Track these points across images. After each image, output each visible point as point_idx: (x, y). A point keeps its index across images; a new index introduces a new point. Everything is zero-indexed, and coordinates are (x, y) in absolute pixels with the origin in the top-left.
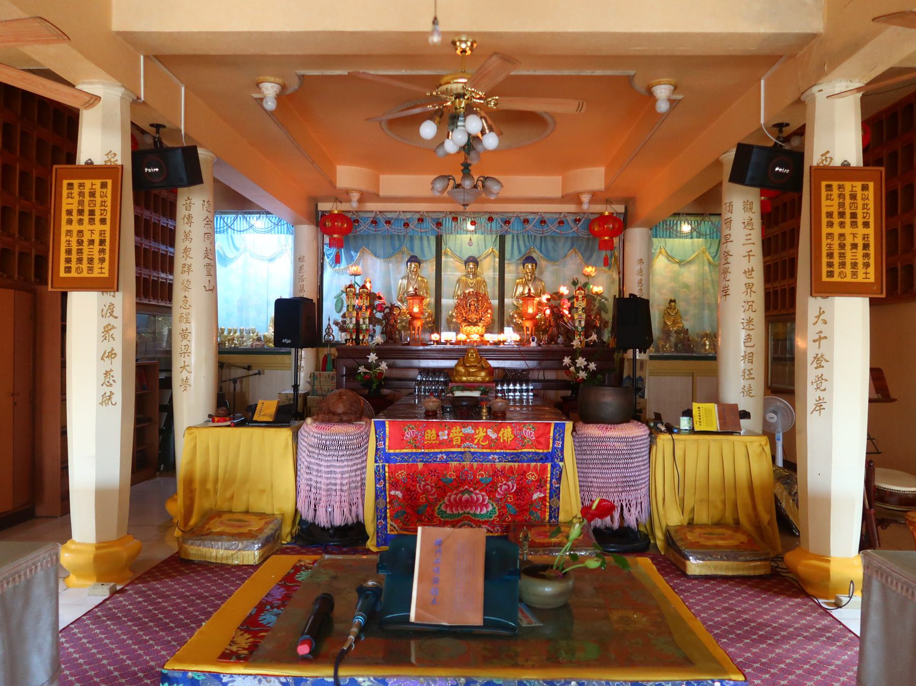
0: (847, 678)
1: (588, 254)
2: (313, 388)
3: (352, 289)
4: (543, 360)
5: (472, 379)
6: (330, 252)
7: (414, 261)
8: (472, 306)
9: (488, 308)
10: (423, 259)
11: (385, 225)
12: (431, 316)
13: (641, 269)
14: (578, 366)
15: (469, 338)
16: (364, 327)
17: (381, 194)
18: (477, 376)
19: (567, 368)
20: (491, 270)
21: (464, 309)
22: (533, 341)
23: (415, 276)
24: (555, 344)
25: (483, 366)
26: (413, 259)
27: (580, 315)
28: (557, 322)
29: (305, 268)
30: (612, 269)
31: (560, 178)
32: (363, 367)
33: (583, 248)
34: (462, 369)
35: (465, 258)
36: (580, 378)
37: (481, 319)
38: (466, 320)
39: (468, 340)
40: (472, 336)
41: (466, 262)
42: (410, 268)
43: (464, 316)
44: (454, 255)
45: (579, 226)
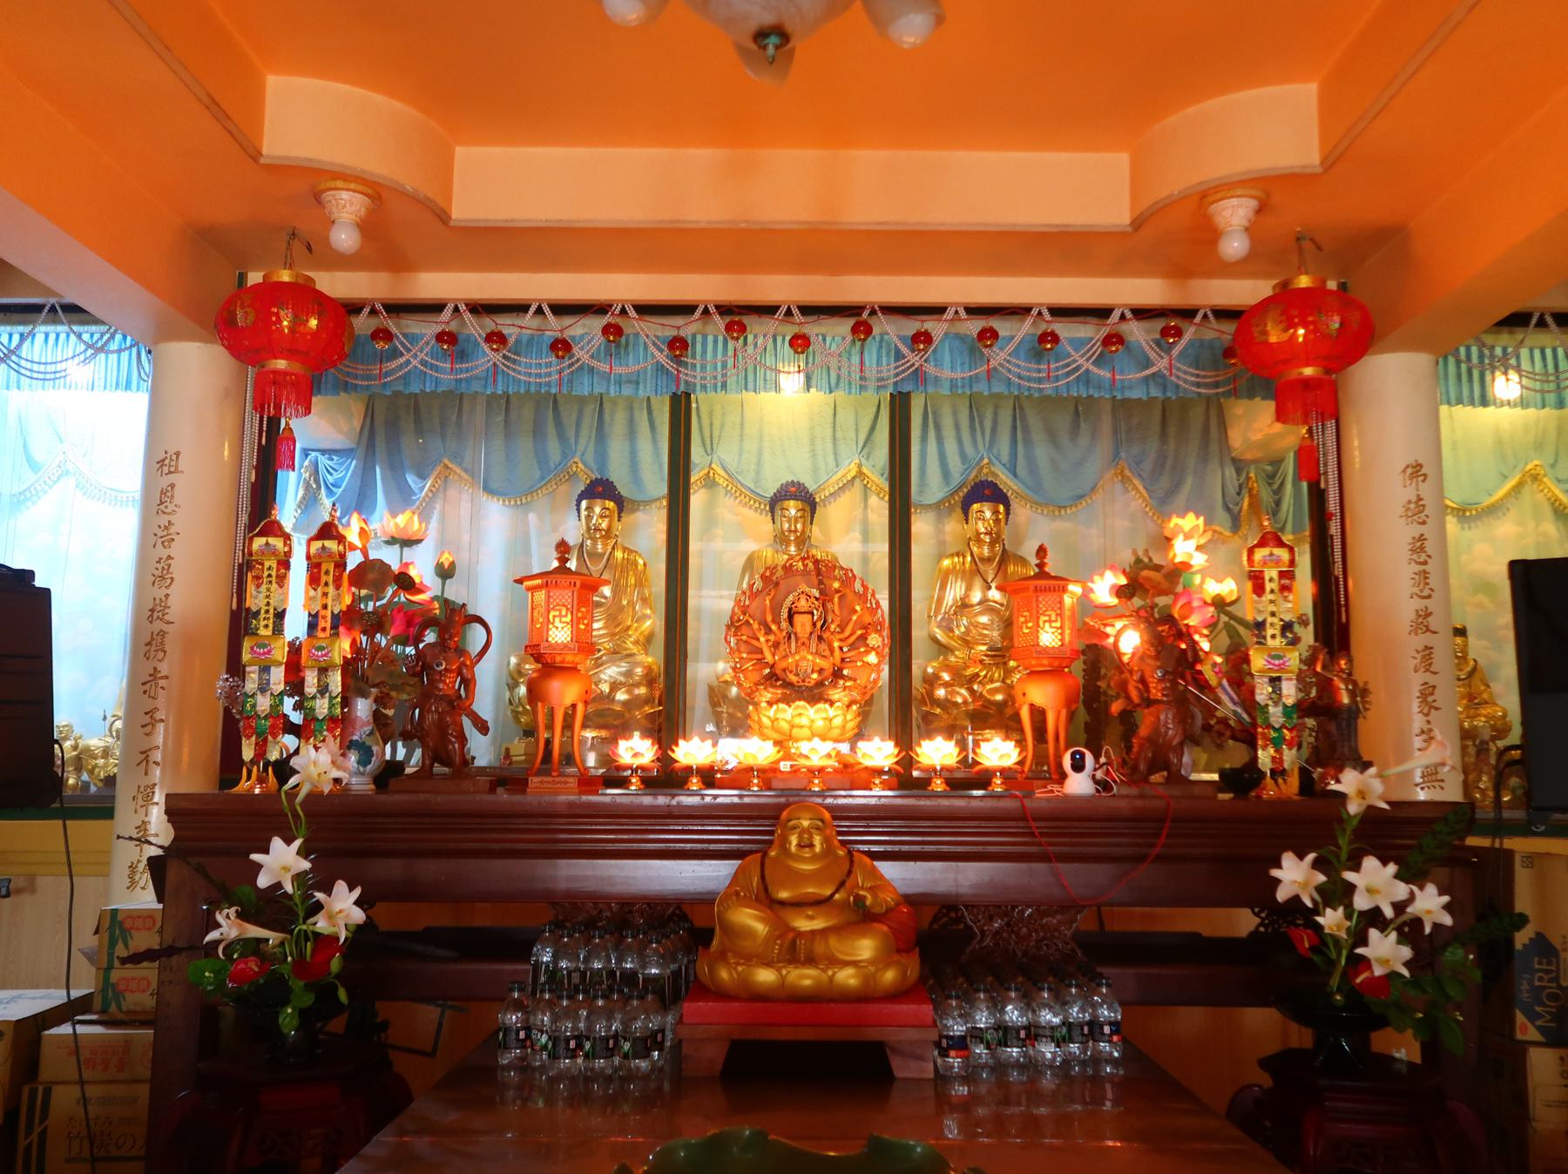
0: (886, 786)
1: (1164, 482)
2: (106, 979)
3: (272, 540)
4: (1141, 859)
5: (805, 978)
6: (337, 476)
8: (798, 619)
10: (639, 497)
11: (486, 347)
12: (650, 680)
13: (1420, 499)
14: (1361, 902)
15: (788, 756)
16: (263, 704)
17: (461, 211)
18: (835, 962)
20: (857, 535)
21: (769, 631)
22: (1078, 766)
23: (605, 545)
24: (1168, 780)
25: (860, 900)
26: (600, 489)
27: (1274, 655)
28: (1175, 684)
29: (180, 495)
30: (1244, 531)
31: (1122, 159)
32: (232, 911)
33: (1147, 465)
34: (750, 920)
35: (770, 490)
36: (1378, 971)
37: (837, 674)
38: (774, 678)
39: (785, 766)
40: (804, 747)
41: (775, 504)
42: (589, 518)
43: (769, 658)
44: (737, 488)
45: (1175, 352)
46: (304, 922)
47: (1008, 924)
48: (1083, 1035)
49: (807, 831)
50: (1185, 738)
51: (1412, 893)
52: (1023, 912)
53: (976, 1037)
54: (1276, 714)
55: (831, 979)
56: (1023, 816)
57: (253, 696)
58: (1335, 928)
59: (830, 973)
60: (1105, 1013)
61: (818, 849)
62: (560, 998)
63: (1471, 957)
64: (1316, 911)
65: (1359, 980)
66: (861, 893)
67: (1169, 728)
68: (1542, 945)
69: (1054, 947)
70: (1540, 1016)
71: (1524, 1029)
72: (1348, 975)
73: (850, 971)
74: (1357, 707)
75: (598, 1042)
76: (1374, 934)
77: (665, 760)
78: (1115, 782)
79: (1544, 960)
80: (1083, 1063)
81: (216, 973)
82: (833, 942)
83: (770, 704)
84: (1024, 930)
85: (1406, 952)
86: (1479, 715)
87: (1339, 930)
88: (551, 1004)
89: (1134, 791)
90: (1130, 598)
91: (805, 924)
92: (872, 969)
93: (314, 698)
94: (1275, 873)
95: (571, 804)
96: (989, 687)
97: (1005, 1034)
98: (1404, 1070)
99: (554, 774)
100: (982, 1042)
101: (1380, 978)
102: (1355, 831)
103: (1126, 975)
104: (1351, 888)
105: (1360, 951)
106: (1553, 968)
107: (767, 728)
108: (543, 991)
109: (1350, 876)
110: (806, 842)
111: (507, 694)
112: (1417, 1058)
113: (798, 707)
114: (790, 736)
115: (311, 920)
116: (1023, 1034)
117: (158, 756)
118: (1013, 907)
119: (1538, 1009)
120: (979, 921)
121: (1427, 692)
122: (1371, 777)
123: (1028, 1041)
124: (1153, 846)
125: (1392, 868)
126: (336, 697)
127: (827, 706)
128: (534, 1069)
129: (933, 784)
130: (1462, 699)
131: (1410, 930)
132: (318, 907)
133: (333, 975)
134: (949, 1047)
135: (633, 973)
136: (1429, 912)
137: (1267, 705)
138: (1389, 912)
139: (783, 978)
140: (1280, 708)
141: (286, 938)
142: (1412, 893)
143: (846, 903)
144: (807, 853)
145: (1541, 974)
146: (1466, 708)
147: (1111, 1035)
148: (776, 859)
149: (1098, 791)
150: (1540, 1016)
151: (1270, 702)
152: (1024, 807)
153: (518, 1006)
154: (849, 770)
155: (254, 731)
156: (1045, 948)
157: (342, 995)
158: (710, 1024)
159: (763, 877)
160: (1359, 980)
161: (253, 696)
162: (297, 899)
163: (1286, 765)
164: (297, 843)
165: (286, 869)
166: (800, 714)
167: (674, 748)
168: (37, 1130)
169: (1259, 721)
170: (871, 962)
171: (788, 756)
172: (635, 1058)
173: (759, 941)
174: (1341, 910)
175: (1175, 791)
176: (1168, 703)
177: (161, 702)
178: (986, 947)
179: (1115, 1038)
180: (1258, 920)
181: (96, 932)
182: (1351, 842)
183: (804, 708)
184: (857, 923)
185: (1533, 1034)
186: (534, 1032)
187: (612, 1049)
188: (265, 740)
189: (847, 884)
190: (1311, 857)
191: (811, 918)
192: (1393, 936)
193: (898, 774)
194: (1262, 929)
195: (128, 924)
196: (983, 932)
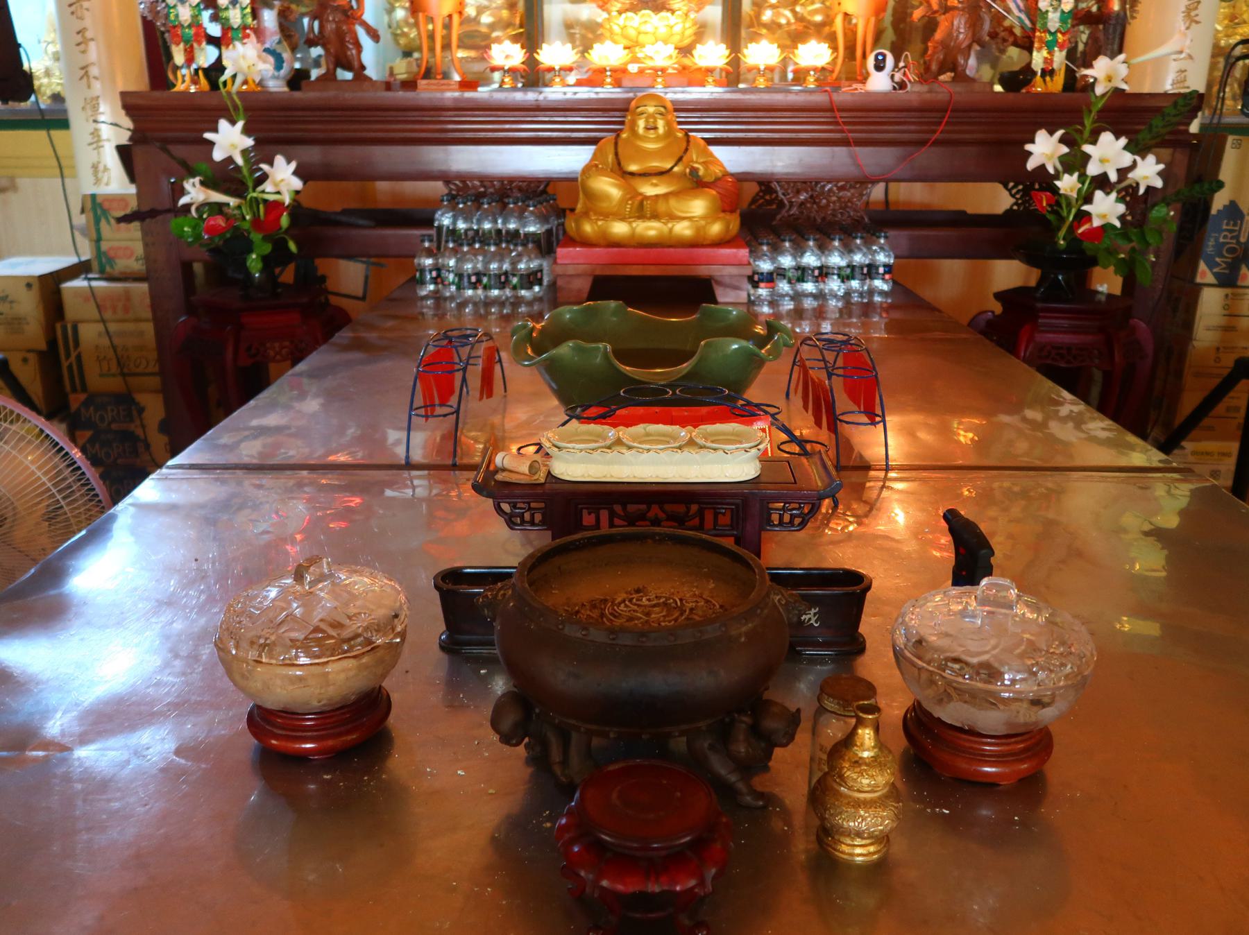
0: (718, 83)
2: (98, 249)
4: (921, 143)
5: (650, 229)
14: (1093, 169)
15: (635, 60)
18: (673, 217)
19: (1044, 179)
22: (879, 67)
24: (954, 79)
25: (694, 171)
34: (608, 187)
36: (1096, 223)
39: (633, 68)
40: (648, 50)
46: (254, 190)
47: (811, 197)
48: (863, 274)
49: (652, 116)
50: (973, 41)
51: (1135, 162)
52: (824, 186)
53: (780, 275)
54: (1054, 21)
55: (671, 230)
56: (831, 108)
57: (175, 6)
58: (1069, 190)
59: (670, 225)
60: (882, 258)
61: (661, 130)
62: (461, 245)
63: (1172, 213)
64: (1057, 176)
65: (1080, 231)
66: (696, 165)
67: (960, 33)
68: (1233, 211)
69: (847, 215)
70: (1218, 265)
71: (1204, 274)
72: (1072, 229)
73: (685, 224)
74: (1125, 14)
75: (492, 277)
76: (1099, 194)
77: (531, 62)
78: (910, 81)
79: (1232, 223)
80: (861, 294)
81: (194, 228)
82: (673, 203)
83: (620, 13)
84: (824, 201)
85: (1121, 208)
86: (1236, 34)
87: (1072, 191)
88: (455, 252)
89: (925, 88)
90: (988, 36)
91: (650, 189)
92: (703, 223)
93: (227, 9)
94: (1028, 147)
95: (455, 100)
96: (810, 8)
97: (802, 273)
98: (1103, 298)
99: (438, 77)
100: (784, 278)
101: (1098, 228)
102: (1100, 111)
103: (902, 236)
104: (1087, 157)
105: (1085, 208)
106: (1237, 228)
107: (617, 34)
108: (447, 242)
109: (1087, 148)
110: (651, 125)
111: (386, 19)
112: (1117, 291)
113: (644, 15)
114: (637, 42)
115: (260, 188)
116: (816, 272)
117: (94, 71)
118: (817, 183)
119: (1218, 259)
120: (789, 194)
121: (1192, 7)
122: (1119, 63)
123: (820, 279)
124: (934, 132)
125: (1123, 141)
126: (246, 8)
127: (669, 14)
128: (446, 299)
129: (757, 82)
130: (1225, 19)
131: (1129, 194)
132: (264, 178)
133: (283, 230)
134: (761, 280)
135: (517, 232)
136: (1146, 178)
137: (1047, 11)
138: (1113, 177)
139: (634, 230)
140: (1058, 14)
141: (242, 203)
142: (1135, 162)
143: (683, 175)
144: (652, 134)
145: (1225, 233)
146: (1227, 27)
147: (883, 275)
148: (627, 140)
149: (894, 88)
150: (1218, 265)
151: (1050, 9)
152: (831, 101)
153: (430, 253)
154: (687, 72)
155: (179, 39)
156: (840, 216)
157: (292, 246)
158: (578, 264)
159: (616, 154)
160: (1080, 231)
161: (175, 6)
162: (245, 172)
163: (1055, 66)
164: (240, 124)
165: (234, 146)
166: (646, 22)
167: (538, 51)
168: (73, 355)
169: (1038, 26)
170: (703, 218)
171: (635, 60)
172: (522, 288)
173: (614, 203)
174: (1076, 175)
175: (958, 88)
176: (963, 9)
177: (88, 22)
178: (792, 215)
179: (887, 277)
180: (1013, 200)
181: (83, 211)
182: (1094, 122)
183: (650, 16)
184: (693, 188)
185: (1210, 279)
186: (443, 272)
187: (504, 283)
188: (192, 47)
189: (684, 159)
190: (1060, 133)
191: (656, 185)
192: (1114, 195)
193: (728, 73)
194: (1015, 207)
195: (106, 205)
196: (791, 203)
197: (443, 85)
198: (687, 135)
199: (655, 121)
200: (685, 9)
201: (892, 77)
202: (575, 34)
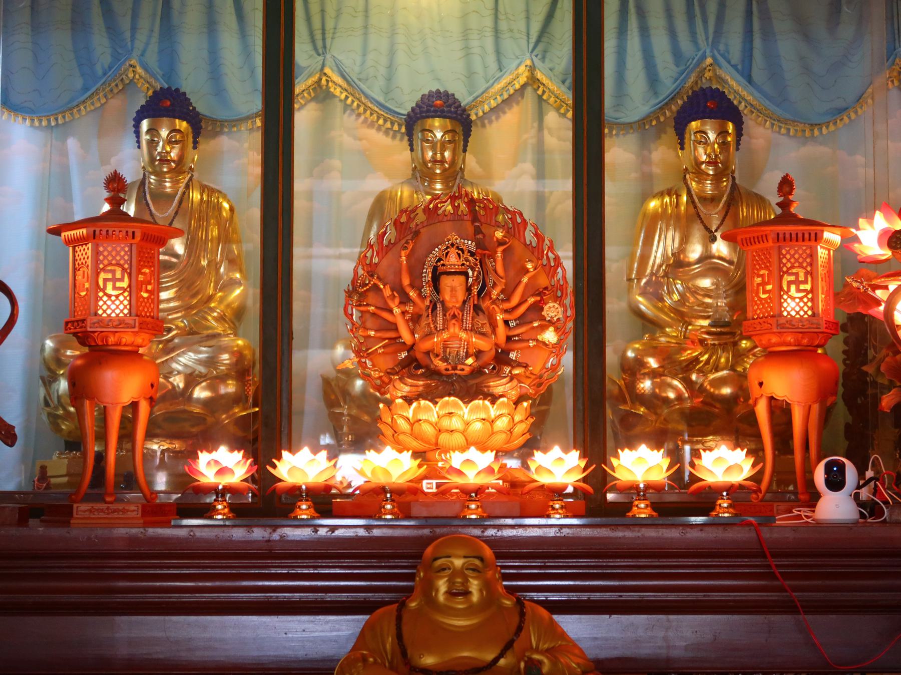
7: (173, 114)
9: (542, 294)
20: (528, 166)
21: (405, 300)
22: (835, 482)
23: (175, 182)
35: (407, 103)
37: (501, 359)
39: (429, 486)
40: (456, 459)
42: (152, 144)
43: (406, 337)
49: (460, 573)
61: (475, 598)
66: (536, 656)
83: (409, 400)
95: (132, 540)
107: (404, 433)
110: (459, 588)
113: (447, 403)
144: (460, 604)
149: (862, 515)
159: (399, 636)
183: (455, 405)
197: (115, 511)
198: (520, 603)
199: (466, 581)
200: (514, 394)
201: (856, 497)
202: (342, 414)
